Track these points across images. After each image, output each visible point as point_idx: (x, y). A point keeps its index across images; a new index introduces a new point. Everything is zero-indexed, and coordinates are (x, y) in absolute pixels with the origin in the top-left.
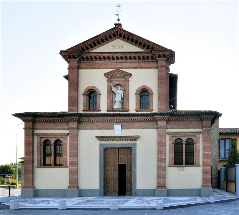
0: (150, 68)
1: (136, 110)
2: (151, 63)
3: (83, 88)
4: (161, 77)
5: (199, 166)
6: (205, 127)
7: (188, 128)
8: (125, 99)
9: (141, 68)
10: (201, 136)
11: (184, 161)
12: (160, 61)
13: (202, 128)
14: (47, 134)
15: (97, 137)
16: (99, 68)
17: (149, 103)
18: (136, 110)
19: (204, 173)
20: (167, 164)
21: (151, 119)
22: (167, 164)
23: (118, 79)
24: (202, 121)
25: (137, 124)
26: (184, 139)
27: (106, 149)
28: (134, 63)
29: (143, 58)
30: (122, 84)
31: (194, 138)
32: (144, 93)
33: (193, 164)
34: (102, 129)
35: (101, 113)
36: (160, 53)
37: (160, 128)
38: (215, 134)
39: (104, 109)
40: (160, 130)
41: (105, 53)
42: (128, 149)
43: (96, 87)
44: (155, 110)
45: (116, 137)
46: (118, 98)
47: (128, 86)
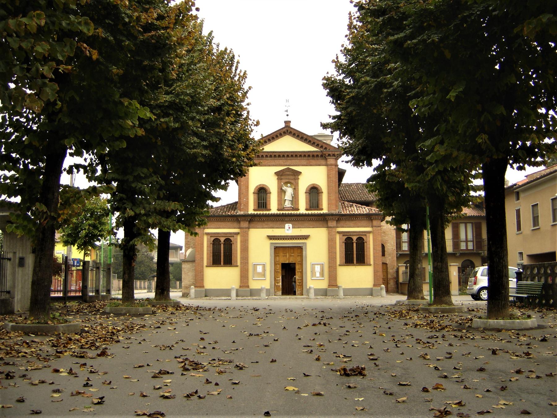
0: (319, 165)
1: (278, 210)
3: (252, 187)
4: (331, 176)
5: (370, 265)
6: (376, 227)
8: (295, 198)
9: (311, 165)
13: (372, 227)
15: (268, 236)
16: (269, 166)
17: (179, 9)
18: (307, 210)
19: (375, 272)
20: (338, 263)
21: (322, 220)
22: (338, 263)
23: (288, 177)
24: (372, 220)
25: (306, 224)
27: (276, 248)
28: (304, 161)
29: (275, 156)
30: (292, 181)
31: (364, 237)
32: (314, 191)
33: (364, 263)
35: (270, 212)
36: (330, 153)
37: (331, 227)
39: (274, 209)
40: (330, 229)
41: (276, 152)
42: (296, 249)
44: (325, 211)
45: (287, 236)
47: (297, 184)
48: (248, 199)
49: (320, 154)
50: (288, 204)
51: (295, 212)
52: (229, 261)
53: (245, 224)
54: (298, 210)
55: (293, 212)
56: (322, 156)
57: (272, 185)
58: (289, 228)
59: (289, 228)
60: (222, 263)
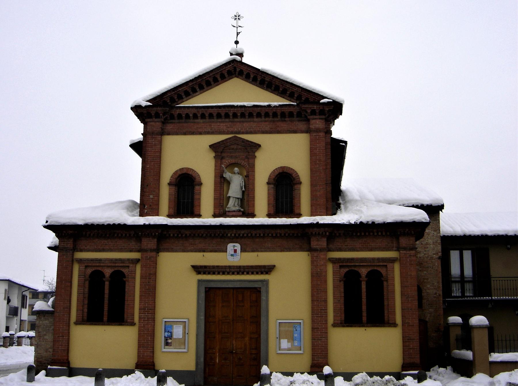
0: (295, 132)
2: (297, 123)
7: (371, 250)
10: (397, 267)
11: (106, 316)
12: (314, 121)
23: (235, 155)
26: (108, 272)
34: (204, 251)
38: (431, 246)
43: (193, 170)
47: (252, 167)
48: (158, 196)
49: (295, 111)
52: (118, 317)
56: (299, 115)
57: (205, 168)
58: (235, 251)
59: (235, 251)
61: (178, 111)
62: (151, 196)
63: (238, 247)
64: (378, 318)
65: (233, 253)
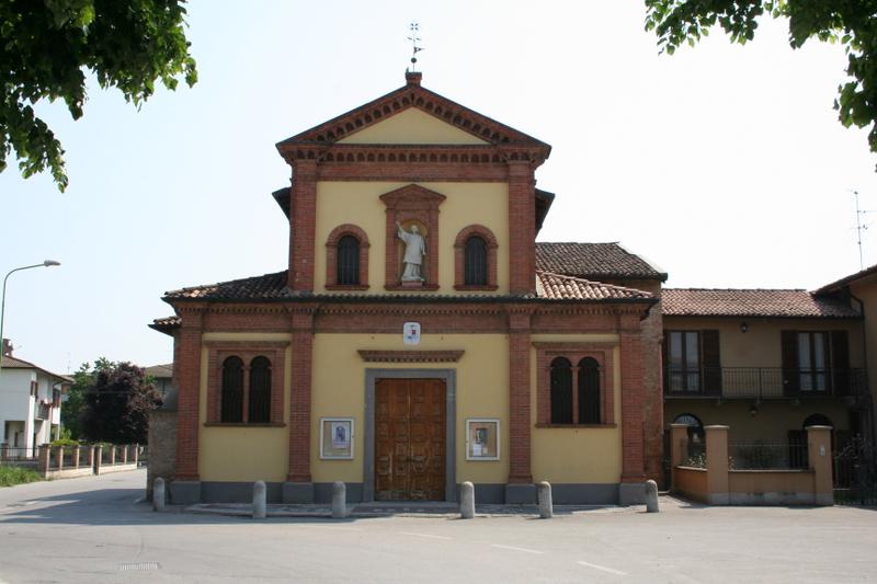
0: (490, 180)
10: (288, 352)
14: (562, 343)
23: (413, 208)
36: (517, 149)
46: (413, 254)
48: (312, 259)
49: (491, 153)
50: (410, 274)
51: (430, 294)
53: (303, 322)
54: (436, 287)
55: (423, 294)
57: (374, 226)
58: (414, 332)
59: (414, 332)
60: (245, 419)
61: (338, 150)
62: (304, 261)
63: (417, 327)
64: (592, 416)
65: (410, 334)
